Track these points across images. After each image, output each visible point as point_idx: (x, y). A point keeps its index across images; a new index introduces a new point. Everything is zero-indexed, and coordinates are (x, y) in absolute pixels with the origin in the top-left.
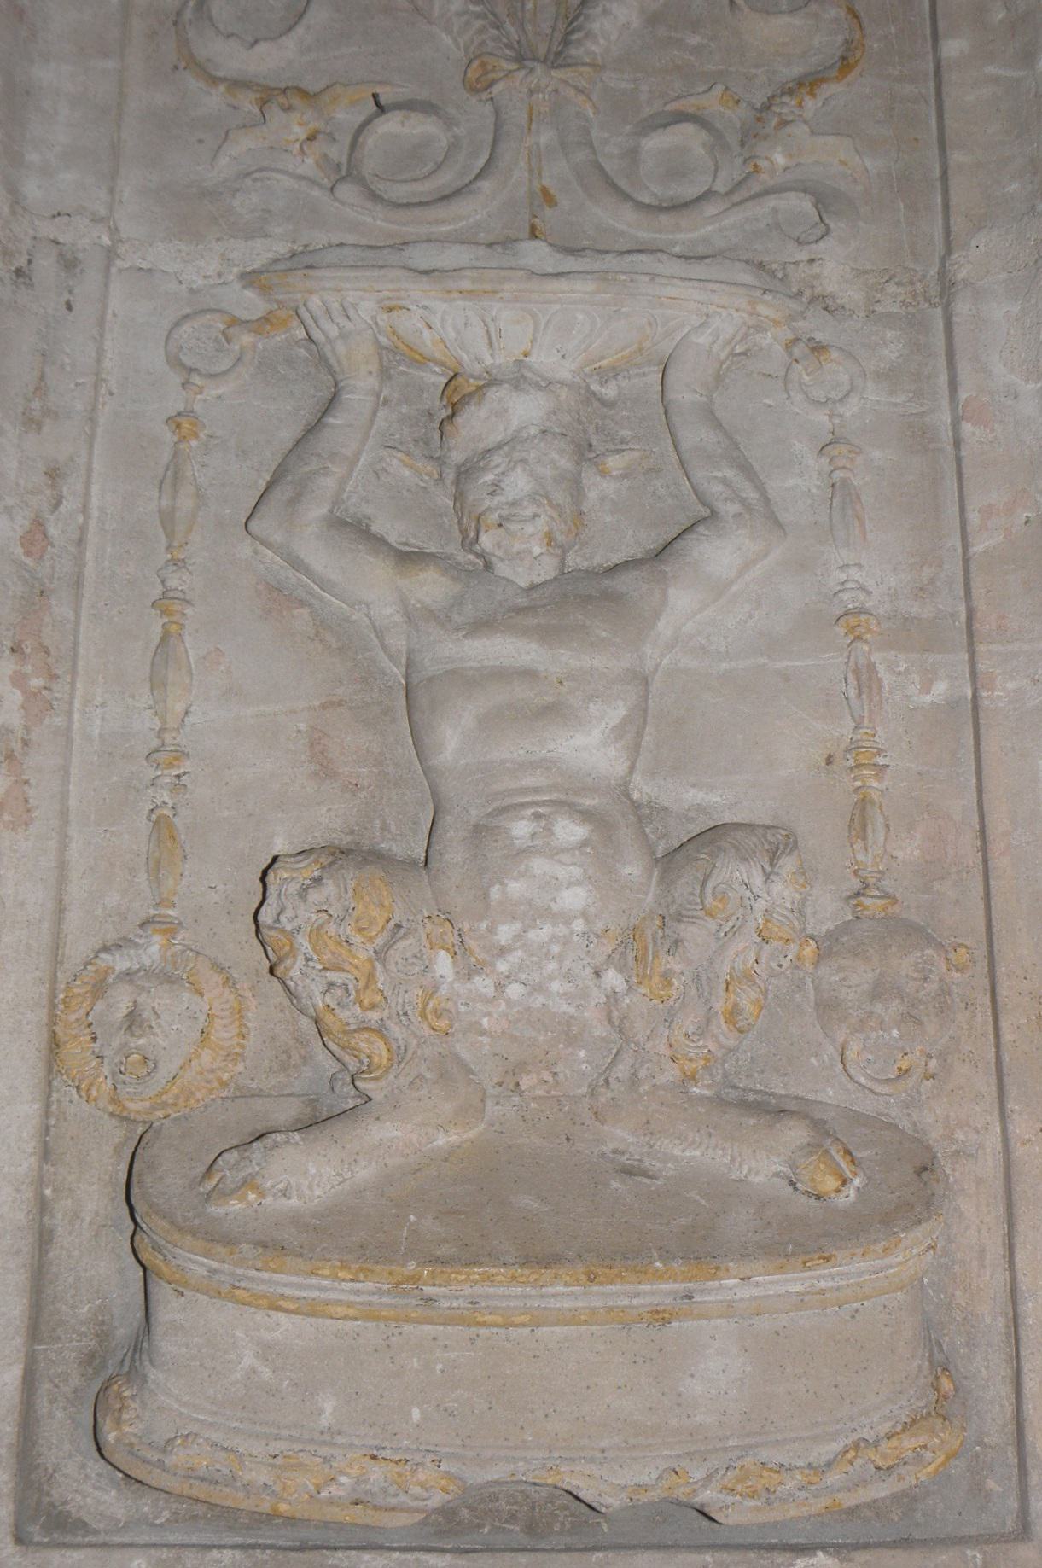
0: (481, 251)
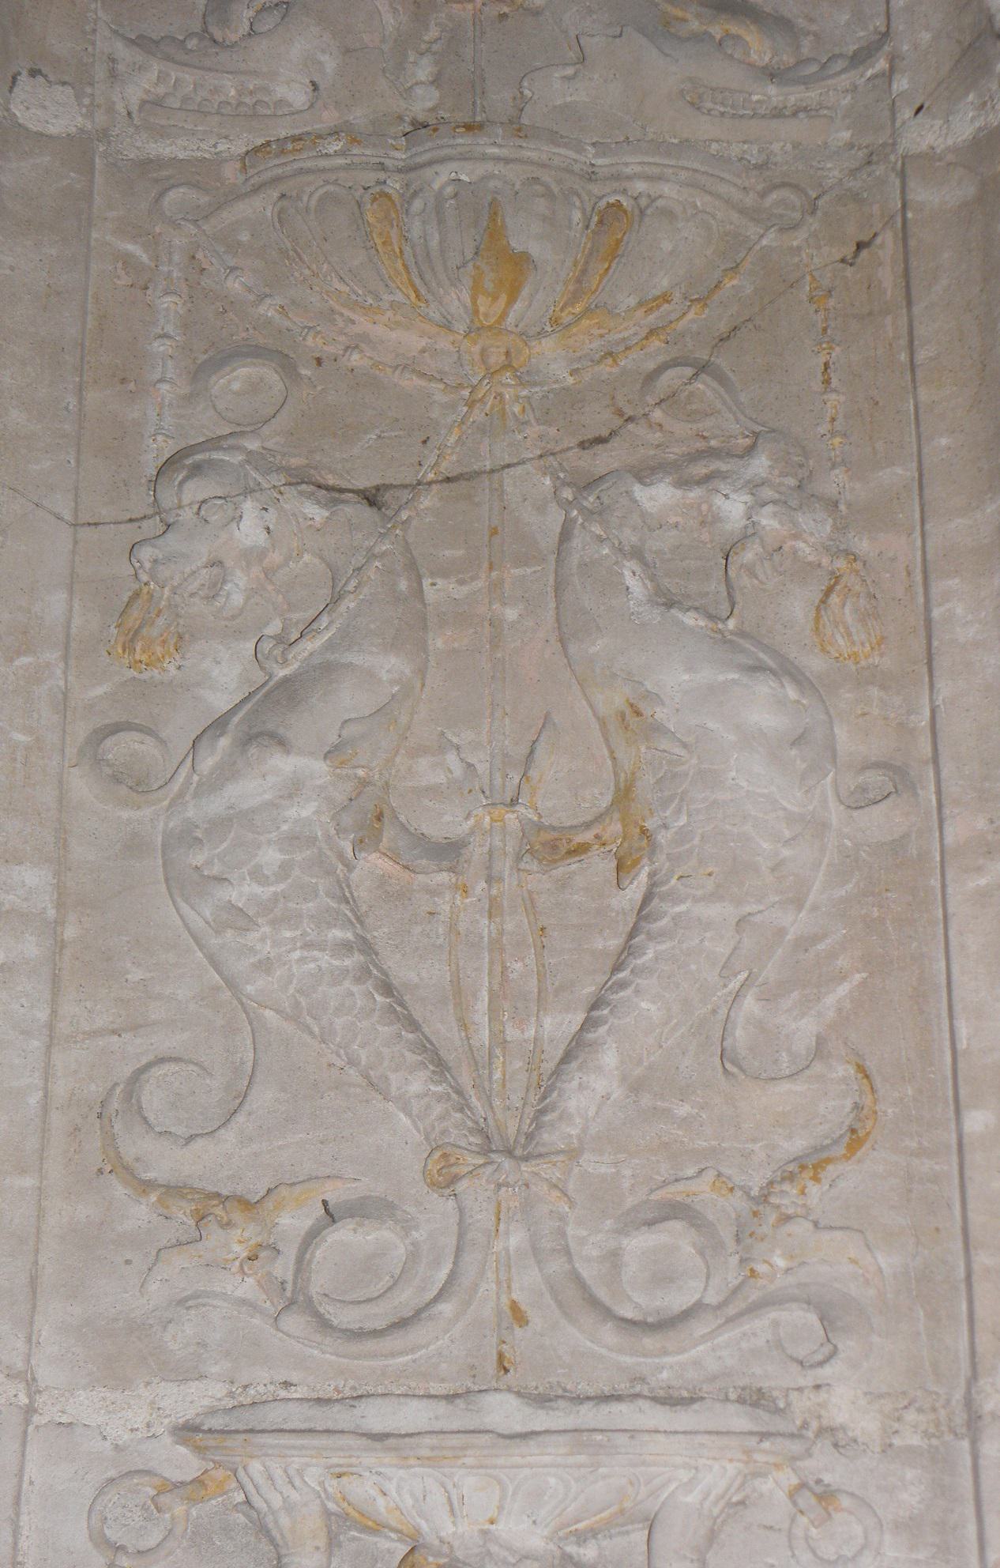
0: (441, 1407)
